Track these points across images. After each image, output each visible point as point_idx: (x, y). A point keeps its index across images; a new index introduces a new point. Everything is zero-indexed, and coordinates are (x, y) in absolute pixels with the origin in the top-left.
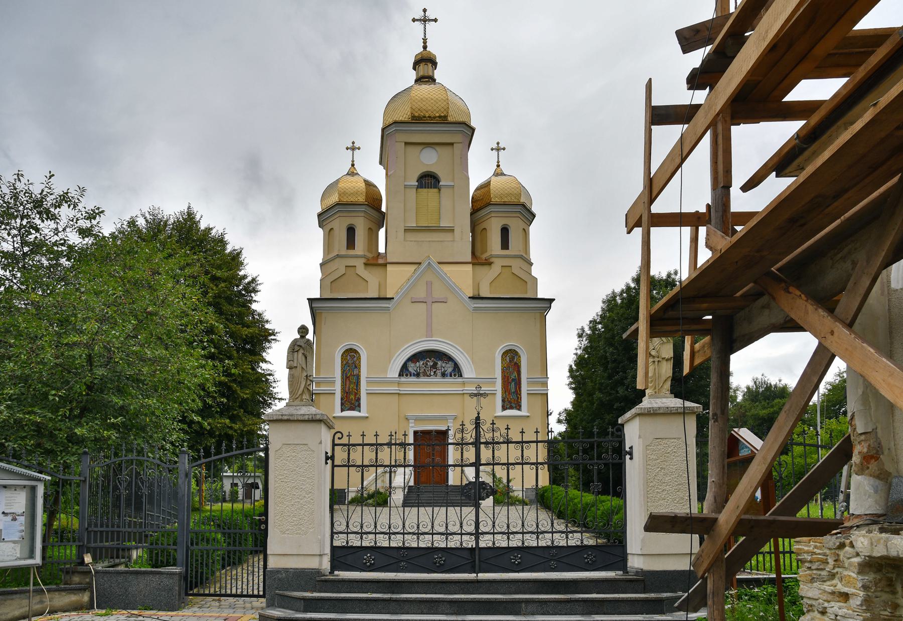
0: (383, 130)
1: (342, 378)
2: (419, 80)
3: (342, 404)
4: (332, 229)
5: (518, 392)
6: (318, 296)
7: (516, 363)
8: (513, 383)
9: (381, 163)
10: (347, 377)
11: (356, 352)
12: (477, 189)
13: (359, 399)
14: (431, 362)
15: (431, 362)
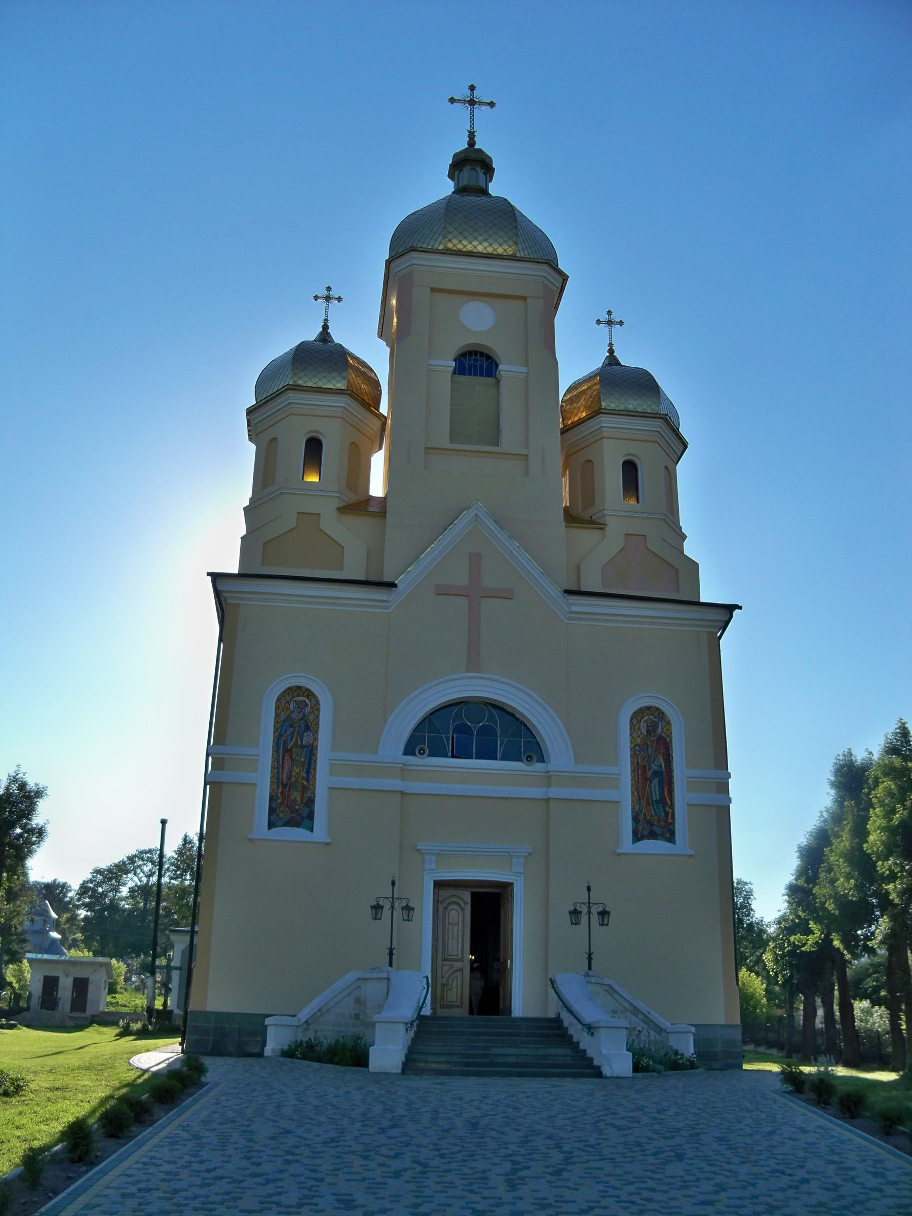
0: (388, 263)
1: (276, 750)
2: (461, 190)
3: (272, 811)
4: (275, 439)
5: (666, 801)
6: (235, 570)
7: (660, 738)
8: (655, 781)
9: (381, 335)
10: (286, 750)
11: (309, 693)
12: (568, 391)
13: (310, 802)
14: (473, 730)
15: (473, 730)
